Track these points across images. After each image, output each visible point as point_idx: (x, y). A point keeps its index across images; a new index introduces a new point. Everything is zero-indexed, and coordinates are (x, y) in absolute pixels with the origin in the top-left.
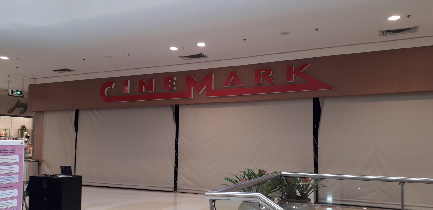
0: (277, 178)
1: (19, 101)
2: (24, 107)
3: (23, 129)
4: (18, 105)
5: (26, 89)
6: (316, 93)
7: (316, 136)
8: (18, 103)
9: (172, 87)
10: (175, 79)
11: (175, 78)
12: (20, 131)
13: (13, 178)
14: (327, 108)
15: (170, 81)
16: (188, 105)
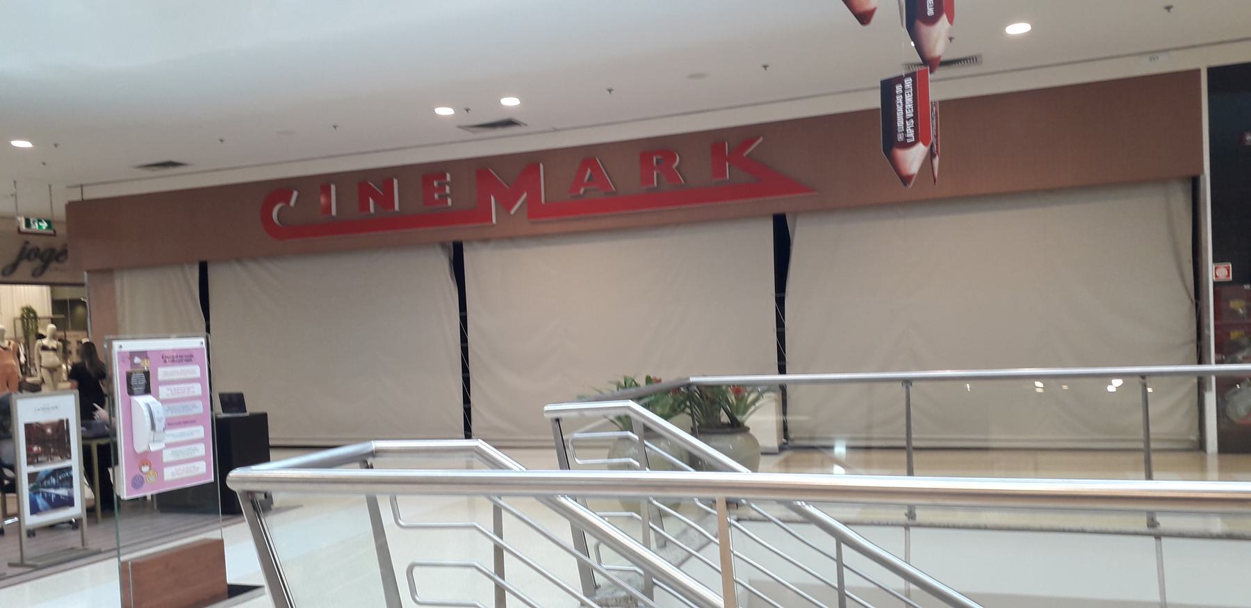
0: (679, 389)
1: (27, 243)
2: (42, 258)
3: (29, 315)
4: (26, 253)
5: (60, 212)
6: (780, 204)
7: (780, 302)
8: (23, 249)
9: (443, 198)
10: (448, 177)
11: (448, 176)
12: (19, 324)
13: (194, 406)
14: (802, 236)
15: (436, 184)
16: (485, 241)
